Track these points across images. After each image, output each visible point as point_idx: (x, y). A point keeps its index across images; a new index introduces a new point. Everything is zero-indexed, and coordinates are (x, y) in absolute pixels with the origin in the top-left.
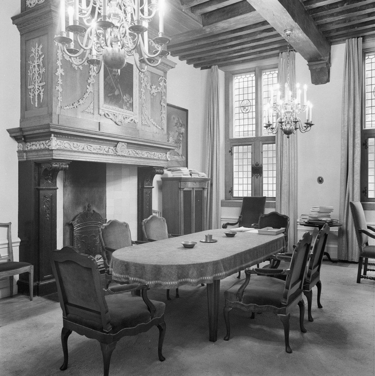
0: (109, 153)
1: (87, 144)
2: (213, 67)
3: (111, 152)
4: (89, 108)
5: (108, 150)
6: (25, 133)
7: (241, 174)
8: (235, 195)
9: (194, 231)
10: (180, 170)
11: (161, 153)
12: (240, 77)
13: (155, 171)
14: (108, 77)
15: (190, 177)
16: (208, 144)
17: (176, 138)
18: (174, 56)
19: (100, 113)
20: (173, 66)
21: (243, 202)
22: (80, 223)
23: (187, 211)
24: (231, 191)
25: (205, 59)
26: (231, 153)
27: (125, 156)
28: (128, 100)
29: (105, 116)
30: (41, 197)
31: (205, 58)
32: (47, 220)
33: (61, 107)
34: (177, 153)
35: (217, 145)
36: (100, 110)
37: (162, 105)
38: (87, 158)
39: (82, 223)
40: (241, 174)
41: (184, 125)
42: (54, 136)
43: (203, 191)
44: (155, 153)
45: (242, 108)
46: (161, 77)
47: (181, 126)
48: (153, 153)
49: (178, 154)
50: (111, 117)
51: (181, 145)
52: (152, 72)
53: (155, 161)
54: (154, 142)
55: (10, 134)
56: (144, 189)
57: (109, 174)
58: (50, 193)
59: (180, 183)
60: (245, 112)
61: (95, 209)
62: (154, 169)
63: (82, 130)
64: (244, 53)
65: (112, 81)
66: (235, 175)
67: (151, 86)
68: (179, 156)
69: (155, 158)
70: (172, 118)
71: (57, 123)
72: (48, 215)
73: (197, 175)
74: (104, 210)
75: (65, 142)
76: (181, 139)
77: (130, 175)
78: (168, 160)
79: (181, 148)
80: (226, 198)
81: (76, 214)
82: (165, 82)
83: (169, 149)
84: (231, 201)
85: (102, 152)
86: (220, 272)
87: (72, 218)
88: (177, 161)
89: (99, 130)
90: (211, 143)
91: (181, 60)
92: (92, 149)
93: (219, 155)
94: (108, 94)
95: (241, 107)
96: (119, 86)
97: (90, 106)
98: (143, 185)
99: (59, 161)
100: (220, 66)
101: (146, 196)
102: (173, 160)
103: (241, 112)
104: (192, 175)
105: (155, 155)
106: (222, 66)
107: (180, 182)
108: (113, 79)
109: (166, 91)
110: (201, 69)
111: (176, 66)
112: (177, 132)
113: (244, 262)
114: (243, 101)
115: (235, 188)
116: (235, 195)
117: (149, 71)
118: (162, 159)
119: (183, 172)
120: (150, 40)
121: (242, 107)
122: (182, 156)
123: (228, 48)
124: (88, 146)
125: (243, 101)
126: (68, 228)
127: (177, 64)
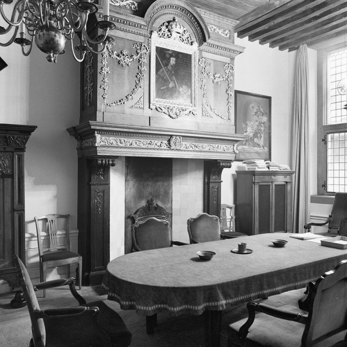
0: (161, 148)
1: (136, 139)
2: (301, 46)
3: (164, 146)
4: (138, 103)
5: (161, 144)
6: (80, 131)
7: (336, 166)
8: (330, 189)
9: (273, 229)
10: (255, 163)
11: (227, 146)
12: (337, 53)
13: (220, 164)
14: (161, 70)
15: (267, 169)
16: (296, 133)
17: (255, 127)
18: (253, 41)
19: (151, 107)
20: (241, 50)
21: (336, 198)
22: (142, 216)
23: (265, 207)
24: (325, 186)
25: (288, 39)
26: (324, 142)
27: (180, 150)
28: (185, 91)
29: (157, 110)
30: (92, 192)
31: (289, 37)
32: (99, 214)
33: (107, 104)
34: (258, 144)
35: (306, 133)
36: (151, 104)
37: (228, 94)
38: (136, 153)
39: (144, 217)
40: (336, 166)
41: (266, 114)
42: (97, 133)
43: (286, 185)
44: (219, 145)
45: (339, 90)
46: (227, 64)
47: (262, 115)
48: (217, 145)
49: (259, 145)
50: (164, 110)
51: (262, 135)
52: (214, 60)
53: (219, 154)
54: (214, 133)
55: (69, 133)
56: (210, 184)
57: (175, 167)
58: (101, 188)
59: (254, 177)
60: (342, 93)
61: (160, 204)
62: (219, 163)
63: (127, 126)
64: (334, 23)
65: (165, 74)
66: (330, 167)
67: (214, 75)
68: (260, 147)
69: (219, 150)
70: (251, 106)
71: (102, 120)
72: (100, 209)
73: (278, 168)
74: (170, 204)
75: (111, 138)
76: (262, 129)
77: (197, 169)
78: (236, 152)
79: (262, 138)
80: (319, 193)
81: (139, 207)
82: (232, 68)
83: (237, 141)
84: (323, 196)
85: (153, 147)
86: (216, 301)
87: (134, 211)
88: (257, 153)
89: (150, 125)
90: (299, 133)
91: (262, 44)
92: (141, 145)
93: (308, 145)
94: (161, 87)
95: (338, 88)
96: (174, 78)
97: (139, 101)
98: (209, 179)
99: (106, 157)
100: (310, 45)
101: (213, 190)
102: (252, 152)
103: (338, 94)
104: (270, 167)
105: (219, 147)
106: (312, 44)
107: (254, 175)
108: (167, 72)
109: (233, 79)
110: (289, 51)
111: (245, 50)
112: (257, 121)
113: (265, 286)
114: (340, 80)
115: (330, 181)
116: (330, 189)
117: (212, 60)
118: (229, 151)
119: (257, 164)
120: (213, 26)
121: (340, 87)
122: (263, 147)
123: (312, 22)
124: (137, 141)
125: (340, 80)
126: (129, 221)
127: (245, 48)
